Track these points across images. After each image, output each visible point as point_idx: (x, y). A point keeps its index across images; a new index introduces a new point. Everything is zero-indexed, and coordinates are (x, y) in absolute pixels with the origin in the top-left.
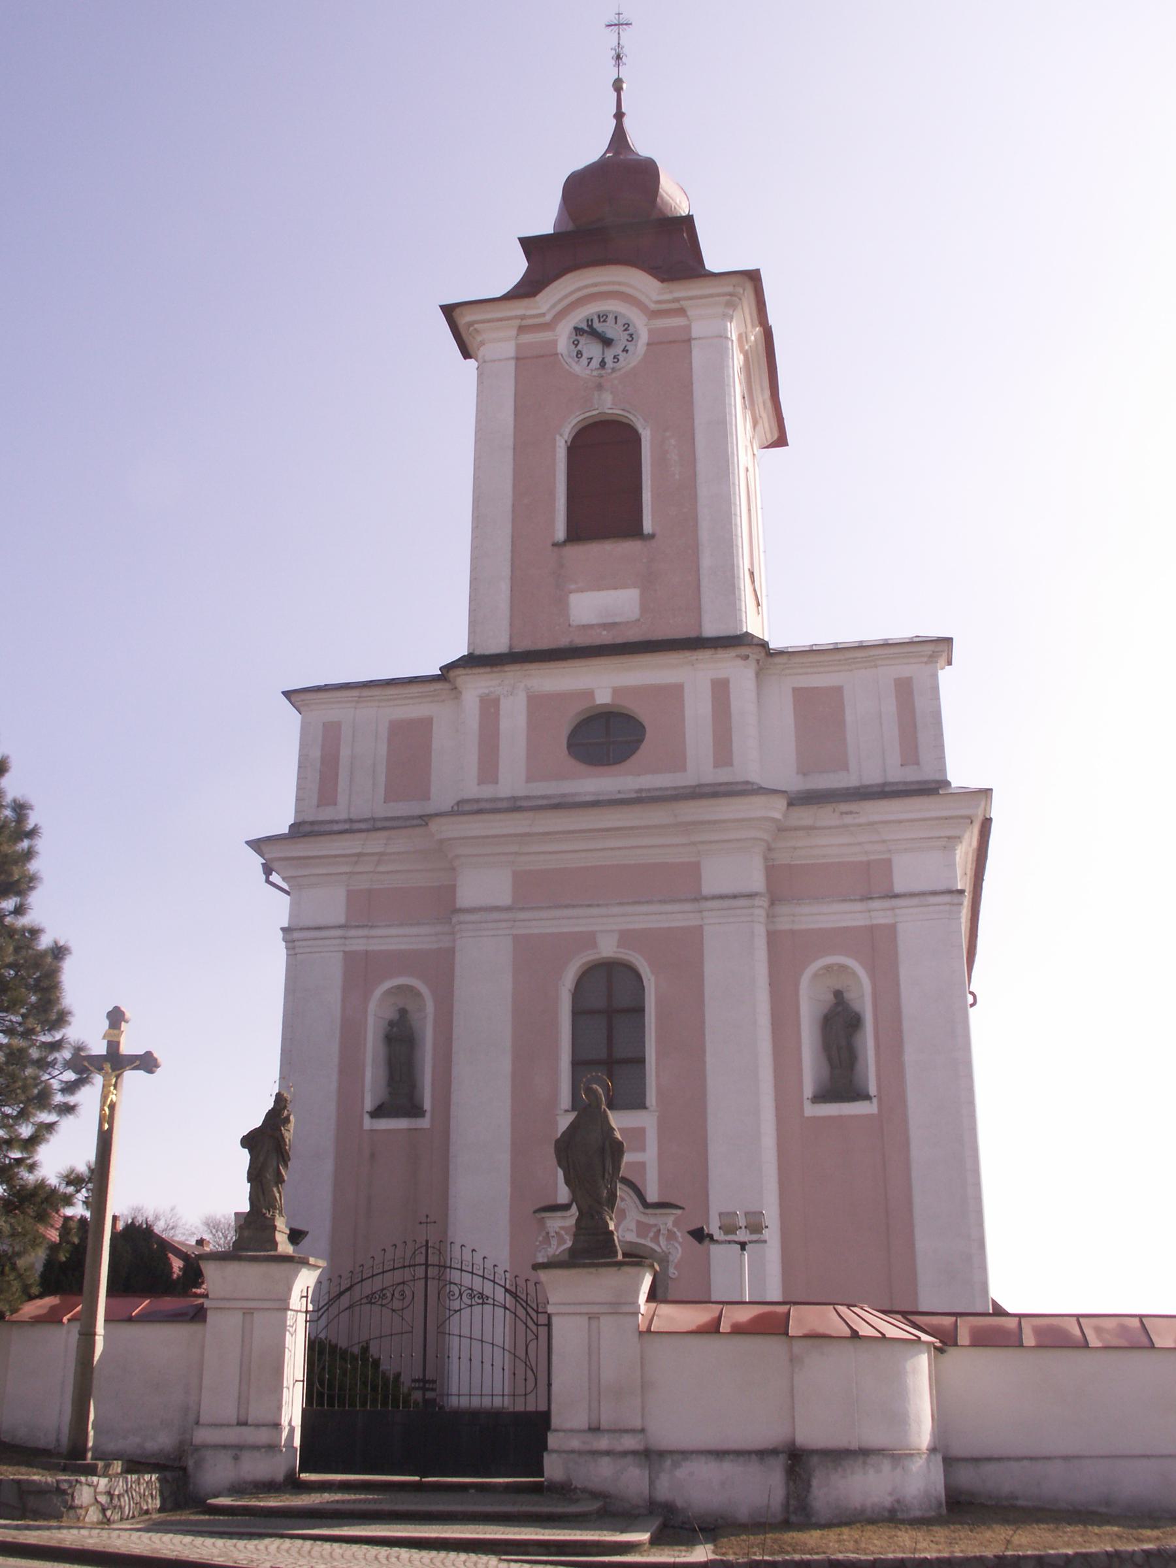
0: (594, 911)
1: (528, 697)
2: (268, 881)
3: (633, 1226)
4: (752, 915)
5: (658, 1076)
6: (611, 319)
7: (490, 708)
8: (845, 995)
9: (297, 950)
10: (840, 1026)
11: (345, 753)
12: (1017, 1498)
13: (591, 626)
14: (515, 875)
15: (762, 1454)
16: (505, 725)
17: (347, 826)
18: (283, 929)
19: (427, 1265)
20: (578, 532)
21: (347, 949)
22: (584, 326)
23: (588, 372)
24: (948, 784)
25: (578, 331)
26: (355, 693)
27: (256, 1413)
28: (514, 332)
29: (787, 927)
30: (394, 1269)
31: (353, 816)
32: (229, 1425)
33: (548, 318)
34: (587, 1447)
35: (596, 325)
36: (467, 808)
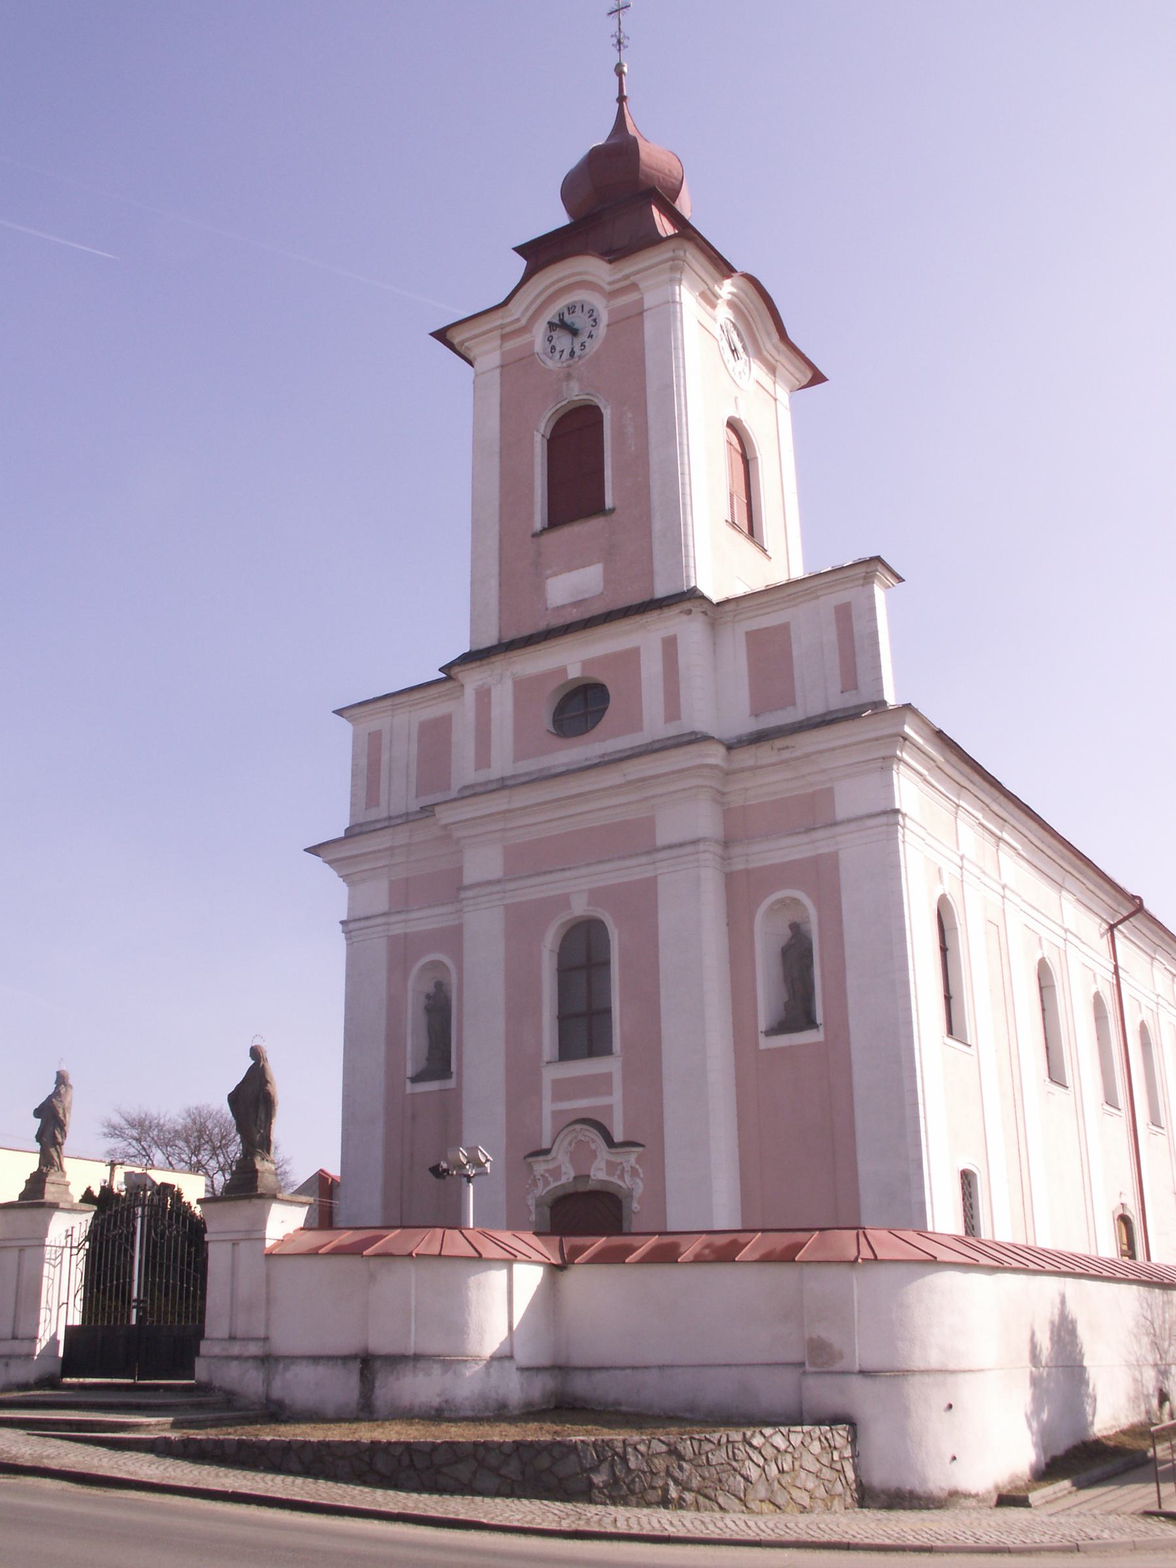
0: (568, 874)
3: (603, 1165)
5: (621, 1024)
6: (578, 309)
7: (484, 697)
10: (797, 957)
11: (385, 757)
12: (620, 1404)
13: (564, 607)
15: (345, 1359)
16: (495, 712)
17: (386, 824)
18: (342, 922)
20: (558, 517)
21: (391, 933)
22: (556, 321)
23: (559, 365)
24: (885, 703)
25: (552, 326)
26: (388, 702)
27: (22, 1331)
28: (498, 342)
29: (741, 867)
31: (392, 814)
32: (5, 1340)
33: (523, 322)
34: (224, 1353)
35: (568, 318)
36: (466, 793)
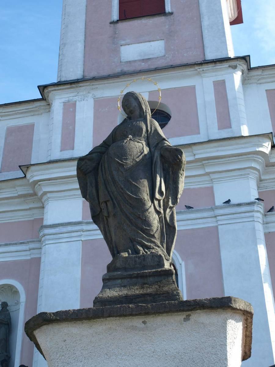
1: (95, 101)
4: (253, 216)
7: (70, 109)
13: (135, 61)
20: (126, 14)
33: (84, 230)
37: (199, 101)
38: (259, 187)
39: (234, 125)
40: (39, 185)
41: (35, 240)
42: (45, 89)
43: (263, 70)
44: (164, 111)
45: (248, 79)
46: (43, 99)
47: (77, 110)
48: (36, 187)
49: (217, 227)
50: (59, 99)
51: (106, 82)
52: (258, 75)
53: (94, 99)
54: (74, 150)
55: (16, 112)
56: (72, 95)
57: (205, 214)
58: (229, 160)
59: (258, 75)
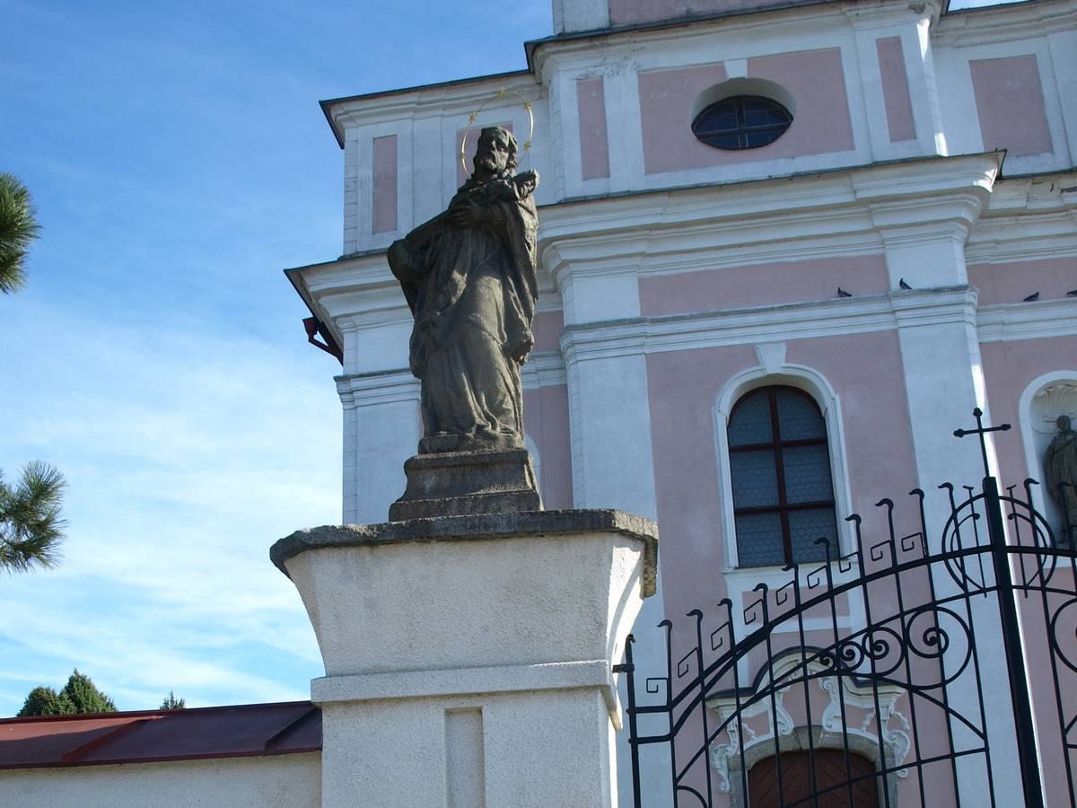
2: (312, 340)
7: (591, 92)
8: (1072, 422)
9: (356, 404)
11: (403, 170)
14: (641, 282)
16: (611, 109)
18: (336, 379)
19: (998, 549)
26: (413, 97)
30: (896, 569)
37: (850, 81)
38: (967, 258)
39: (921, 132)
40: (554, 247)
41: (547, 353)
42: (538, 50)
43: (968, 17)
44: (774, 102)
45: (937, 37)
46: (530, 72)
47: (606, 95)
48: (545, 251)
49: (895, 332)
50: (566, 73)
51: (660, 35)
52: (956, 29)
53: (638, 72)
54: (611, 179)
55: (474, 99)
56: (594, 62)
57: (875, 307)
58: (920, 203)
59: (956, 29)
